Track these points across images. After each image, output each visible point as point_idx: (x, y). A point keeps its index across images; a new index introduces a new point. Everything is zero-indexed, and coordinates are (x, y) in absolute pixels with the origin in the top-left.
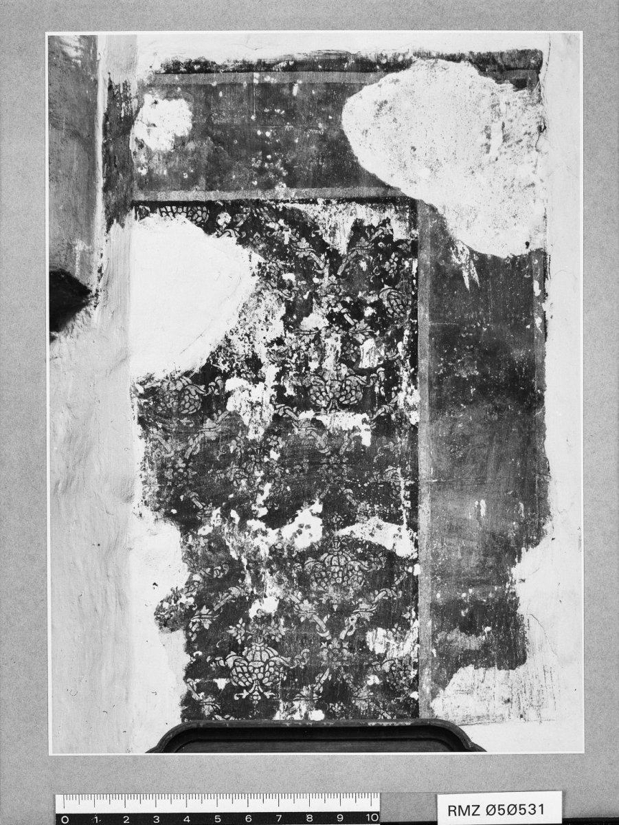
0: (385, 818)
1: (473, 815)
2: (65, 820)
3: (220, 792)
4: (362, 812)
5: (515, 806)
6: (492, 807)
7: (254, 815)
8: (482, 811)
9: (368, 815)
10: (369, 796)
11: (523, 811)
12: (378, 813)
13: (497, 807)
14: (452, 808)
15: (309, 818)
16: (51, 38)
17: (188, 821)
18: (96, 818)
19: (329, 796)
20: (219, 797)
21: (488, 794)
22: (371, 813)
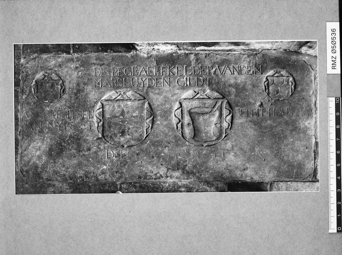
0: (339, 95)
1: (336, 59)
2: (339, 229)
3: (328, 213)
5: (332, 41)
8: (334, 55)
10: (329, 134)
11: (334, 38)
12: (336, 98)
14: (333, 68)
15: (338, 127)
16: (14, 44)
17: (339, 177)
18: (338, 216)
20: (329, 133)
22: (336, 101)
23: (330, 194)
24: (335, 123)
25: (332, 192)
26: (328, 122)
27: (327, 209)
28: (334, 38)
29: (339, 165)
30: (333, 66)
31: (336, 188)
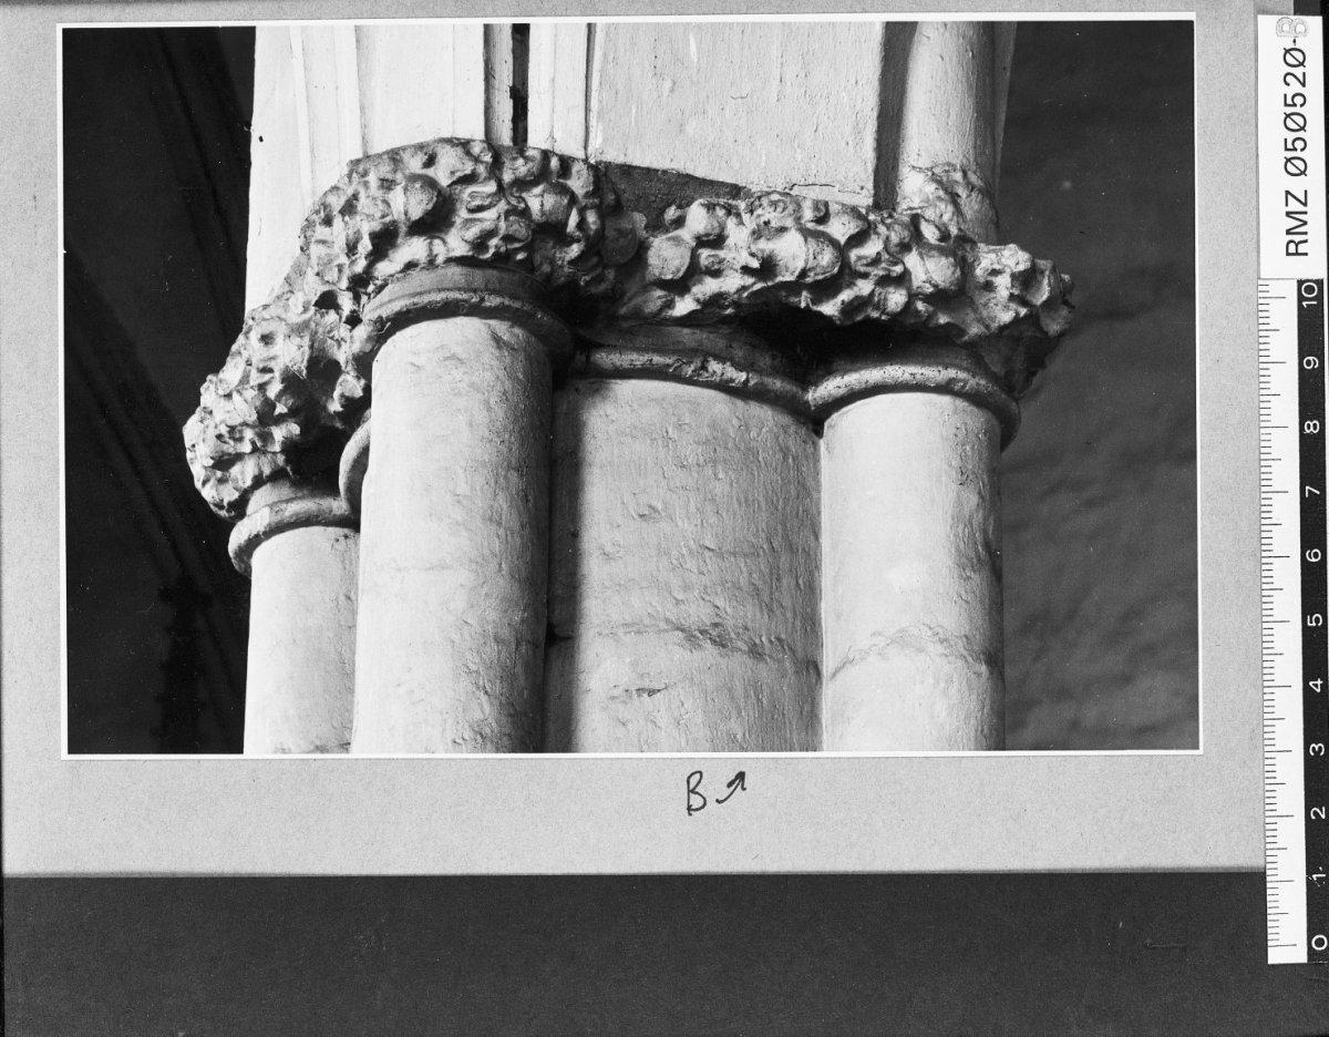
1: (1305, 204)
2: (1320, 943)
4: (1304, 635)
6: (1288, 56)
7: (1310, 801)
9: (1304, 304)
10: (1265, 366)
11: (1299, 100)
14: (1292, 248)
17: (1319, 682)
18: (1314, 876)
20: (1269, 456)
22: (1301, 298)
23: (1269, 508)
25: (1274, 306)
26: (1261, 480)
28: (1299, 100)
29: (1317, 620)
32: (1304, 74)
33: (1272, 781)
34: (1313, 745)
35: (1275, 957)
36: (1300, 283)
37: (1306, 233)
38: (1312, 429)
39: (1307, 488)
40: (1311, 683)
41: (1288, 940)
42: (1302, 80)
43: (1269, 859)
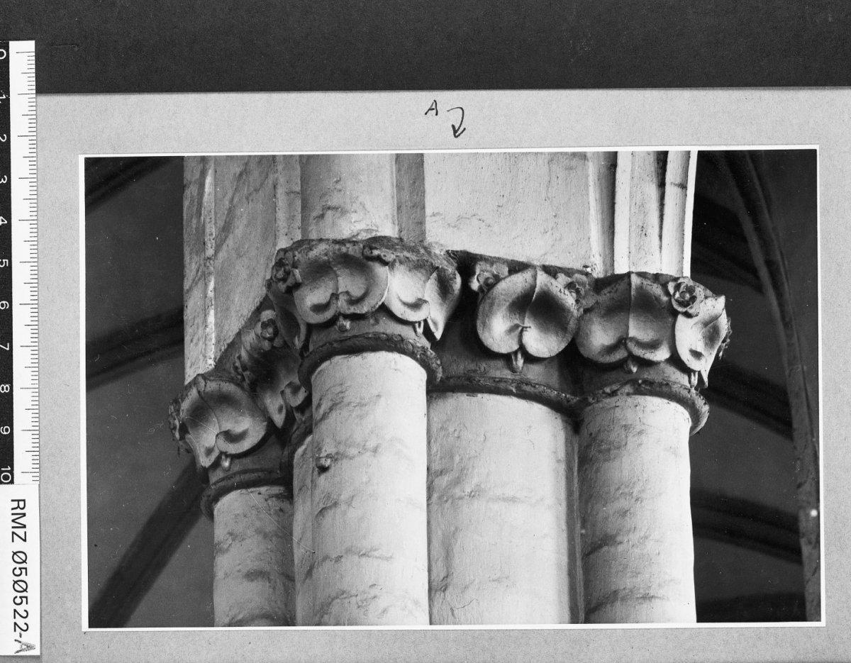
1: (13, 533)
4: (12, 339)
5: (24, 562)
9: (9, 469)
13: (24, 594)
14: (21, 504)
18: (4, 97)
19: (33, 247)
21: (39, 625)
22: (12, 472)
23: (33, 314)
24: (12, 161)
25: (29, 467)
26: (39, 468)
27: (42, 356)
28: (18, 601)
30: (23, 509)
31: (12, 188)
32: (15, 618)
33: (32, 159)
34: (5, 182)
35: (30, 45)
36: (12, 482)
37: (13, 514)
38: (5, 390)
39: (8, 349)
40: (6, 222)
41: (22, 55)
42: (16, 614)
43: (34, 100)
